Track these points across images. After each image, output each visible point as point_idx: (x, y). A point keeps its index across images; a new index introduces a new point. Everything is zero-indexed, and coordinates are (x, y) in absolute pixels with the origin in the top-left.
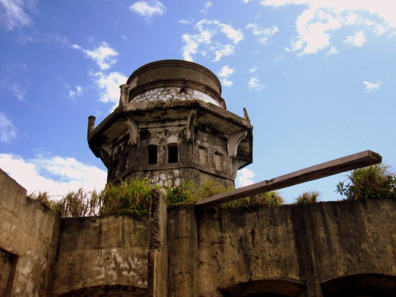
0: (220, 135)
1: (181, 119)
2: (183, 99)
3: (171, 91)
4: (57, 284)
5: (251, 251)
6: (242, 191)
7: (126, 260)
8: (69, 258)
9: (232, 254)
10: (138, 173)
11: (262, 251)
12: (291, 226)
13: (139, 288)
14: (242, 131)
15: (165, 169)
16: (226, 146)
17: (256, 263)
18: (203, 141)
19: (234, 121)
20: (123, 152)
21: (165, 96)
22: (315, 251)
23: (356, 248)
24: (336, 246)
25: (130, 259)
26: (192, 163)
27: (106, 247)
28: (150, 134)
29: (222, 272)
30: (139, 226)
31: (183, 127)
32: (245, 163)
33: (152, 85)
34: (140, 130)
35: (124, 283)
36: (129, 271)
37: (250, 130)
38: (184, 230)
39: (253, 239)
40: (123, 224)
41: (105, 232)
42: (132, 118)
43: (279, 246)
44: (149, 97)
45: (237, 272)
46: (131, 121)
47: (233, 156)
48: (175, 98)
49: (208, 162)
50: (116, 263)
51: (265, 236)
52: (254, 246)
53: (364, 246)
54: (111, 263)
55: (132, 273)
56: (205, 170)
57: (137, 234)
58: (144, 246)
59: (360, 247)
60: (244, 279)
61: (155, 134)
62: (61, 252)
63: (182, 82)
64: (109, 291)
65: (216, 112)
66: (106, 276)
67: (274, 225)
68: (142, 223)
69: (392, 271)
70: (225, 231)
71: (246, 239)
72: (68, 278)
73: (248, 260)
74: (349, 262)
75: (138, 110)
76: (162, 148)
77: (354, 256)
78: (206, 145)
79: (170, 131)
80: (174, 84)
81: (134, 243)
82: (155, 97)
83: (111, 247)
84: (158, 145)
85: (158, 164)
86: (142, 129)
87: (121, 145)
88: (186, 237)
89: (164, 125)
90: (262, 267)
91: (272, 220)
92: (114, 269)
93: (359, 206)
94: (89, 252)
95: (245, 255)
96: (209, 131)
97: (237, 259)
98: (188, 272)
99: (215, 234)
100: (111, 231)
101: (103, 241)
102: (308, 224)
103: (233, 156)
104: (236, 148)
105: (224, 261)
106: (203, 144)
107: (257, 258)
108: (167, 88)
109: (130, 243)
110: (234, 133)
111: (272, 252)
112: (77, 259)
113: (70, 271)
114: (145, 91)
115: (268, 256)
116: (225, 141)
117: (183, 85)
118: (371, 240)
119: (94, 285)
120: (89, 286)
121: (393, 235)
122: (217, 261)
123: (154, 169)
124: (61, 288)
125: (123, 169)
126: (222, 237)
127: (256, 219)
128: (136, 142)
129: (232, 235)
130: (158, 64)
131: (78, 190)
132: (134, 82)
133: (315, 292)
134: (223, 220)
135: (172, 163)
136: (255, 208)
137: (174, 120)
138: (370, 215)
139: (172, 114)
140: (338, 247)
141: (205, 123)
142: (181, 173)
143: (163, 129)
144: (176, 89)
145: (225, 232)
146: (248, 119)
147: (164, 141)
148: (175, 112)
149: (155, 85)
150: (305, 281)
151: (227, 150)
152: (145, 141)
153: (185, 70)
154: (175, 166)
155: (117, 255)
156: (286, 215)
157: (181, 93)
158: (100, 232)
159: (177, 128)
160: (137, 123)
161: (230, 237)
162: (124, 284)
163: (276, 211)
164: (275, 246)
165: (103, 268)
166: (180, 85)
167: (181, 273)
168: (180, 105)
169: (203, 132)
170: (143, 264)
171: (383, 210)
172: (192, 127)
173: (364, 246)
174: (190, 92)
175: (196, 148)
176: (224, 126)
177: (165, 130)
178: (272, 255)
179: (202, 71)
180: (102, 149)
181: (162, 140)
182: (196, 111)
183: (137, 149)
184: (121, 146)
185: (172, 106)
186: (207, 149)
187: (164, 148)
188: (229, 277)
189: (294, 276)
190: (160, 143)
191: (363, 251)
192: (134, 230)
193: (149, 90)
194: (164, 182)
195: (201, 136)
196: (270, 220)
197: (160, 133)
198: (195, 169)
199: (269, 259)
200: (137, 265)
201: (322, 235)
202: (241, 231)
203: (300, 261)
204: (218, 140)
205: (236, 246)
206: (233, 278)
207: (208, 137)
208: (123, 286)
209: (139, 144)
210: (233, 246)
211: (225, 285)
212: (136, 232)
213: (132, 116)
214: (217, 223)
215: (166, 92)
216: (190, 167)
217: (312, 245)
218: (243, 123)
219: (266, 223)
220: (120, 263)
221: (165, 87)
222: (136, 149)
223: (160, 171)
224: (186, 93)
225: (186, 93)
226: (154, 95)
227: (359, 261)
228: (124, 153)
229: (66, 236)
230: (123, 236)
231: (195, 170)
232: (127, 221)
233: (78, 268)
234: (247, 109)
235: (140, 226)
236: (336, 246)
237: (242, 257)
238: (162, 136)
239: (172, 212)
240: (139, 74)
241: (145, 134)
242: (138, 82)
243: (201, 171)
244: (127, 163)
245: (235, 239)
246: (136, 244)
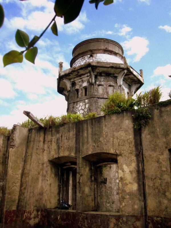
0: (112, 75)
3: (85, 58)
12: (75, 131)
15: (82, 100)
21: (83, 62)
22: (82, 143)
23: (98, 140)
24: (90, 140)
34: (71, 82)
39: (61, 139)
42: (66, 78)
46: (65, 79)
49: (103, 92)
53: (101, 139)
56: (101, 97)
59: (99, 140)
61: (78, 83)
63: (90, 51)
65: (102, 65)
67: (69, 132)
69: (110, 151)
71: (59, 139)
73: (59, 148)
74: (94, 147)
77: (96, 144)
80: (87, 54)
82: (79, 63)
84: (79, 88)
86: (72, 82)
90: (63, 151)
93: (102, 119)
95: (58, 146)
96: (104, 75)
102: (81, 130)
106: (101, 83)
107: (62, 147)
108: (84, 57)
110: (120, 72)
114: (75, 61)
115: (65, 146)
116: (116, 78)
117: (90, 53)
118: (104, 136)
121: (114, 133)
129: (55, 137)
130: (80, 44)
131: (45, 118)
133: (79, 162)
138: (106, 123)
139: (81, 72)
140: (90, 140)
143: (81, 80)
144: (88, 56)
149: (77, 57)
150: (76, 157)
153: (92, 44)
156: (74, 126)
157: (90, 58)
159: (87, 78)
160: (70, 79)
166: (89, 53)
167: (29, 156)
171: (113, 119)
173: (101, 139)
175: (96, 86)
176: (112, 71)
178: (67, 145)
179: (102, 41)
180: (64, 93)
181: (81, 86)
182: (90, 68)
185: (79, 68)
189: (73, 154)
190: (80, 87)
191: (100, 142)
194: (82, 107)
196: (68, 130)
197: (80, 82)
198: (95, 97)
201: (85, 135)
202: (58, 135)
203: (76, 147)
205: (56, 142)
206: (53, 156)
207: (104, 79)
210: (55, 142)
214: (51, 133)
215: (83, 59)
217: (81, 140)
218: (121, 67)
221: (82, 56)
223: (80, 102)
225: (93, 57)
226: (79, 62)
227: (98, 146)
231: (95, 98)
236: (90, 140)
237: (57, 147)
238: (80, 84)
239: (31, 131)
241: (74, 84)
243: (98, 98)
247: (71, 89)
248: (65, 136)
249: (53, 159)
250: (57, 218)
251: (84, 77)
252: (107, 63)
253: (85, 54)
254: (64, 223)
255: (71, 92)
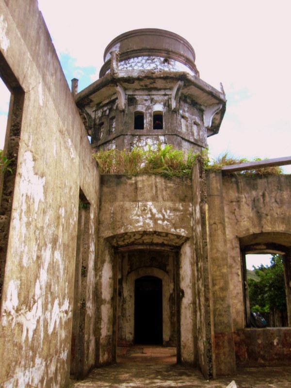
1: (167, 89)
2: (166, 69)
3: (155, 60)
4: (102, 229)
5: (262, 209)
6: (272, 162)
7: (160, 211)
8: (110, 208)
9: (246, 211)
10: (127, 136)
11: (270, 210)
13: (172, 234)
14: (218, 104)
16: (202, 116)
17: (266, 219)
18: (184, 111)
19: (214, 94)
20: (108, 115)
25: (163, 211)
26: (177, 131)
27: (142, 201)
28: (137, 100)
29: (239, 224)
30: (169, 185)
31: (168, 97)
32: (212, 133)
33: (137, 53)
34: (127, 96)
35: (159, 230)
36: (163, 220)
37: (223, 103)
38: (215, 189)
39: (264, 200)
40: (156, 182)
41: (141, 188)
42: (121, 84)
43: (284, 207)
44: (133, 65)
45: (251, 225)
46: (120, 87)
47: (209, 126)
48: (159, 67)
50: (152, 213)
51: (273, 198)
52: (265, 206)
54: (147, 213)
55: (166, 222)
57: (168, 191)
58: (175, 201)
60: (257, 230)
62: (103, 203)
63: (166, 52)
64: (145, 235)
66: (144, 224)
67: (281, 190)
68: (172, 182)
70: (241, 192)
71: (258, 200)
72: (111, 224)
73: (259, 216)
75: (129, 77)
76: (148, 115)
78: (187, 115)
79: (155, 99)
80: (159, 54)
81: (166, 198)
82: (140, 64)
83: (147, 201)
84: (144, 111)
85: (145, 129)
86: (129, 95)
87: (105, 109)
88: (218, 196)
89: (150, 93)
90: (271, 222)
91: (279, 186)
92: (150, 218)
94: (127, 204)
95: (258, 212)
97: (251, 215)
98: (220, 223)
99: (233, 194)
100: (145, 188)
101: (139, 195)
103: (209, 126)
104: (211, 119)
105: (241, 216)
106: (184, 113)
107: (267, 215)
108: (151, 57)
109: (163, 198)
111: (279, 211)
112: (118, 209)
113: (113, 219)
114: (129, 58)
116: (201, 112)
117: (166, 55)
119: (134, 231)
120: (130, 231)
122: (235, 216)
123: (141, 134)
124: (106, 232)
125: (109, 132)
126: (239, 197)
127: (266, 184)
128: (124, 107)
129: (247, 196)
132: (116, 47)
134: (239, 184)
135: (159, 130)
136: (266, 175)
137: (160, 90)
139: (160, 84)
141: (187, 94)
142: (166, 139)
143: (149, 97)
144: (160, 59)
145: (241, 193)
146: (224, 94)
147: (150, 108)
148: (163, 81)
151: (203, 120)
152: (132, 107)
153: (167, 40)
154: (162, 133)
155: (152, 207)
157: (164, 63)
158: (136, 188)
159: (162, 97)
160: (125, 89)
161: (245, 198)
162: (160, 231)
163: (283, 179)
164: (281, 207)
165: (141, 217)
166: (164, 54)
167: (215, 223)
168: (168, 75)
169: (184, 103)
170: (174, 215)
172: (177, 97)
174: (172, 63)
175: (179, 117)
176: (203, 98)
177: (151, 98)
178: (278, 213)
179: (182, 42)
180: (86, 111)
181: (149, 108)
182: (183, 82)
183: (125, 114)
184: (106, 111)
185: (162, 76)
186: (187, 118)
187: (150, 116)
188: (245, 229)
190: (146, 110)
192: (166, 188)
193: (134, 58)
194: (150, 146)
195: (183, 107)
197: (146, 100)
198: (179, 136)
199: (276, 216)
200: (169, 216)
202: (254, 193)
204: (196, 110)
205: (251, 205)
206: (248, 230)
207: (188, 108)
208: (159, 232)
209: (126, 110)
210: (248, 205)
211: (242, 235)
212: (168, 190)
213: (122, 83)
214: (235, 186)
215: (150, 61)
216: (175, 137)
219: (274, 188)
220: (155, 214)
221: (149, 56)
222: (124, 115)
223: (147, 136)
224: (169, 63)
226: (139, 62)
228: (110, 117)
229: (105, 189)
230: (156, 192)
231: (179, 138)
232: (160, 181)
233: (119, 216)
234: (223, 84)
235: (171, 185)
237: (255, 214)
238: (148, 103)
240: (122, 41)
241: (131, 101)
242: (120, 48)
243: (183, 139)
244: (113, 126)
245: (250, 199)
246: (168, 199)
247: (125, 107)
248: (271, 197)
249: (247, 234)
250: (272, 344)
251: (157, 95)
252: (209, 86)
253: (156, 54)
254: (288, 349)
255: (127, 114)
